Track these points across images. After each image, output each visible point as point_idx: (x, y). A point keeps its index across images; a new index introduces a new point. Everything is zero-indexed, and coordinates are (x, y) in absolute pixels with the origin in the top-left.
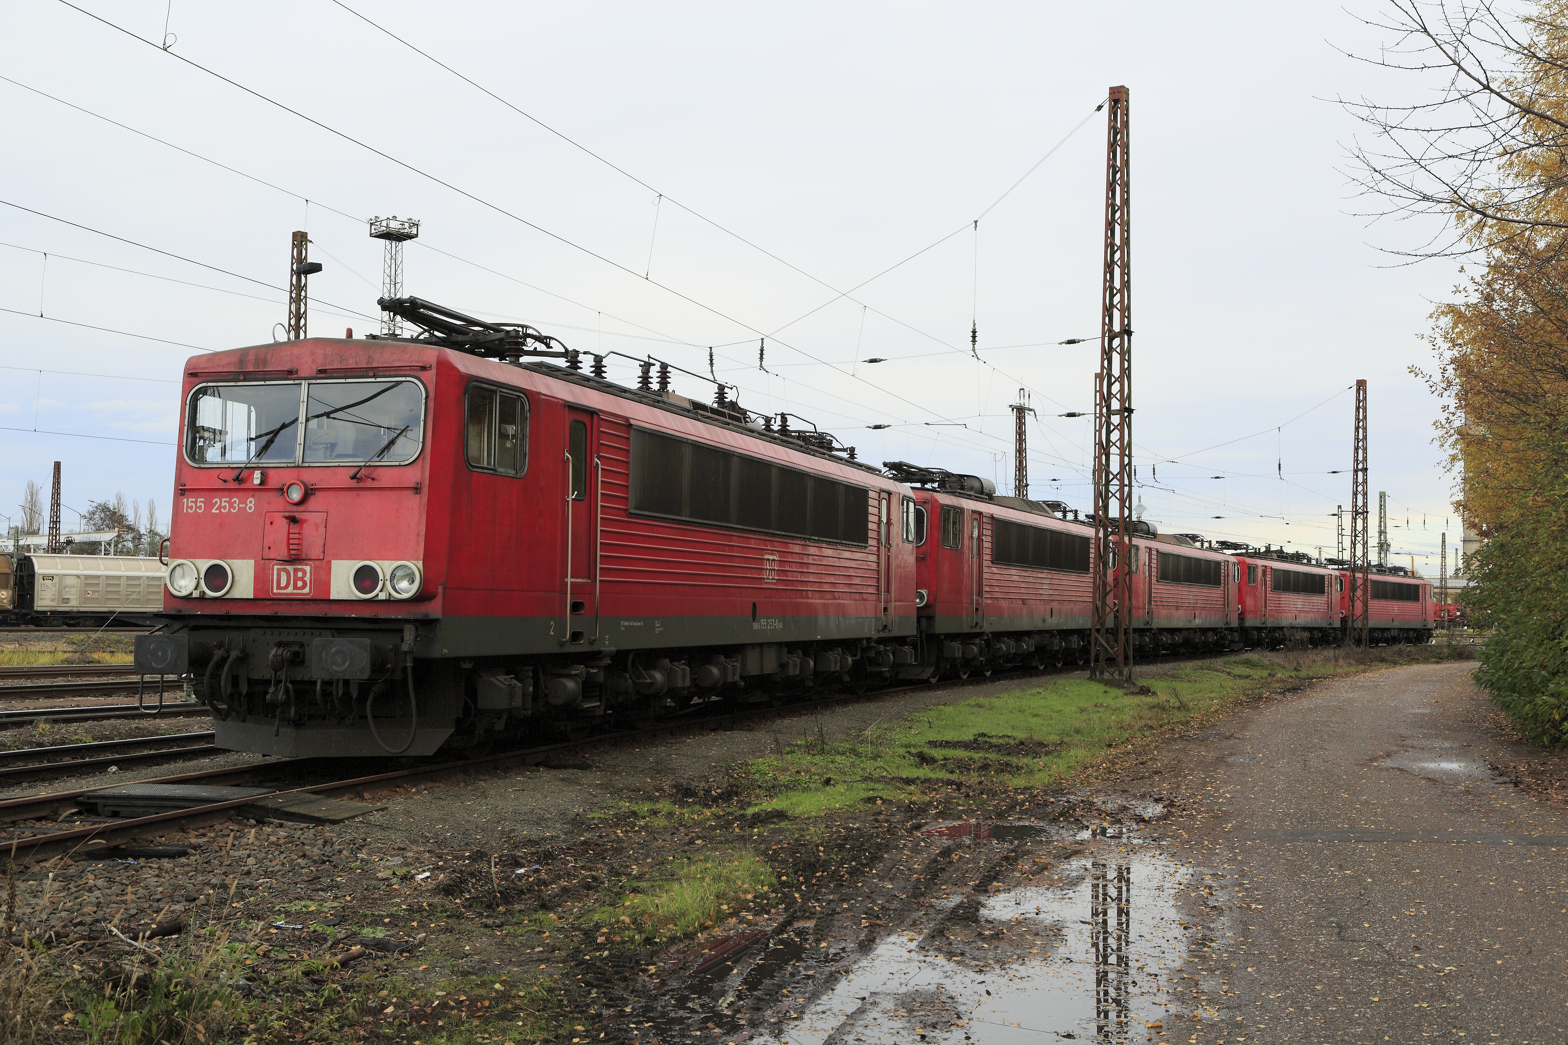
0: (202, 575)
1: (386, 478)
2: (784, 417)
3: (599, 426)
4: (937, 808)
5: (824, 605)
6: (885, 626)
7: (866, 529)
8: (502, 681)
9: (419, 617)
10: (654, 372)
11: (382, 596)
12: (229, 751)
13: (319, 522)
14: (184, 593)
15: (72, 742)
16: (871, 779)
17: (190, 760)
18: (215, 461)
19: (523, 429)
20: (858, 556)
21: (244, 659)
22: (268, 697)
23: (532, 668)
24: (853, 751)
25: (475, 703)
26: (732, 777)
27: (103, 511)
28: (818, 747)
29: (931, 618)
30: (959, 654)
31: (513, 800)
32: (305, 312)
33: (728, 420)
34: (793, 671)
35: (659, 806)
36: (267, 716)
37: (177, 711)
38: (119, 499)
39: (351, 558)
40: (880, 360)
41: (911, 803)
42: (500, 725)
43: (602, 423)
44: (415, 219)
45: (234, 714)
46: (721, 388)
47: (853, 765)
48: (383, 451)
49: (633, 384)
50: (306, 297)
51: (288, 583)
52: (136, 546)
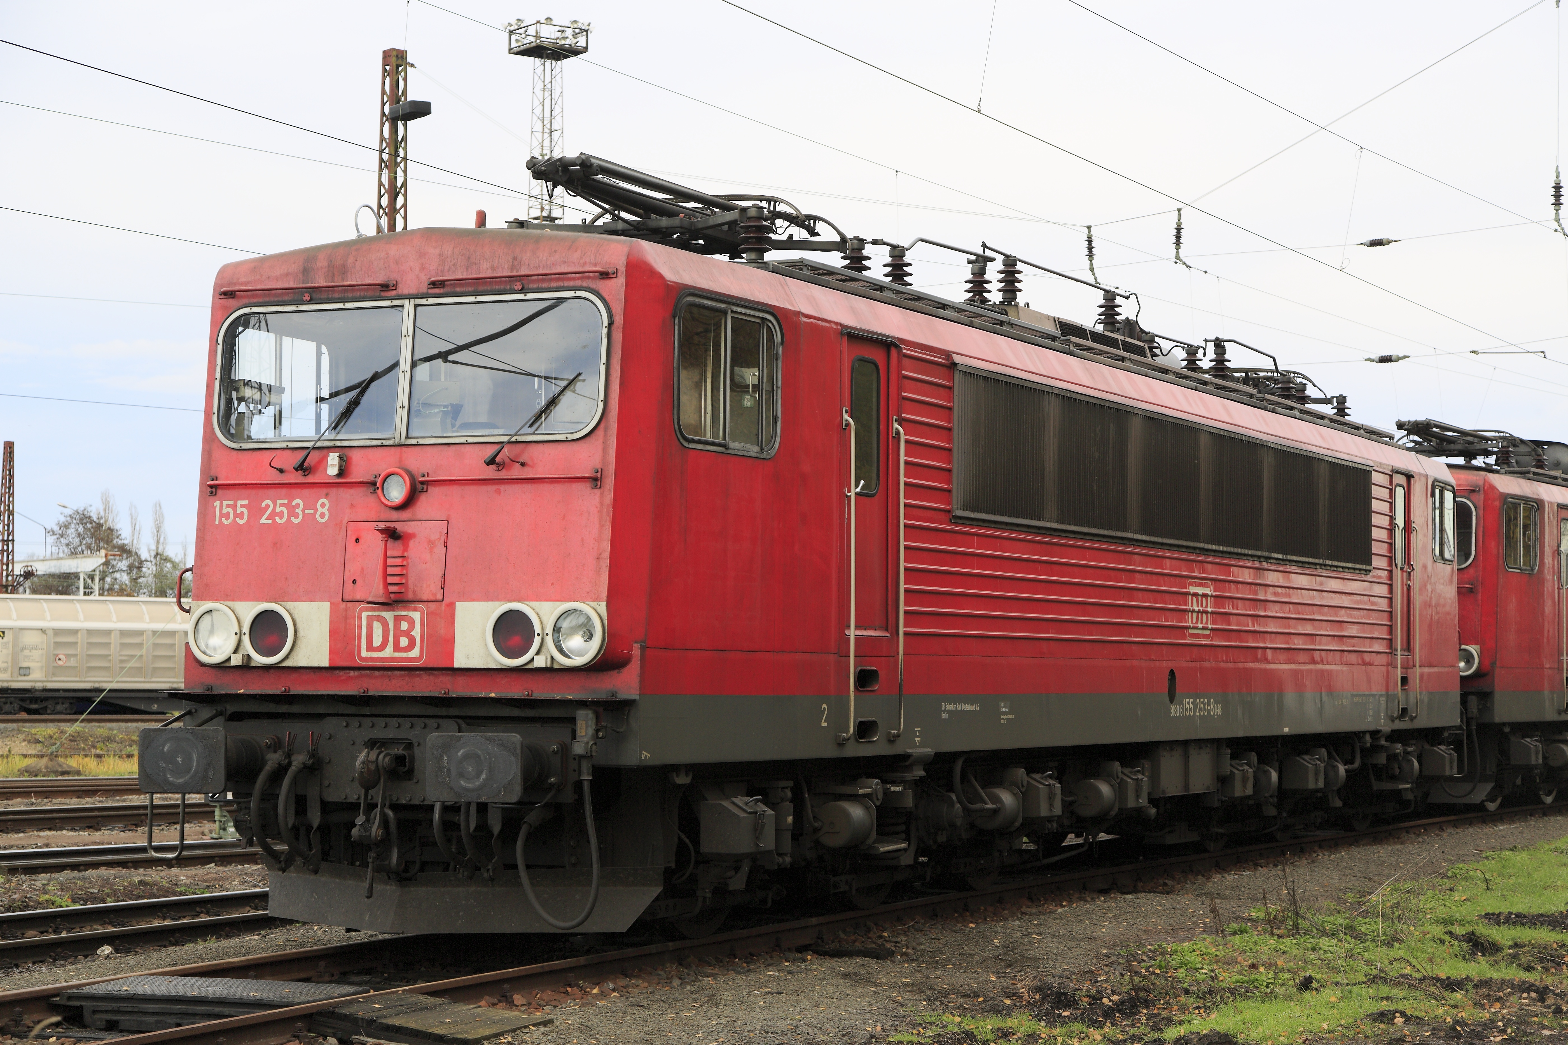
0: (246, 629)
1: (544, 462)
2: (1219, 345)
3: (900, 368)
4: (1504, 1031)
5: (1295, 672)
6: (1404, 711)
7: (1368, 539)
8: (741, 805)
9: (602, 696)
10: (993, 272)
11: (540, 662)
12: (290, 922)
13: (434, 537)
14: (217, 658)
15: (39, 905)
16: (1385, 980)
17: (228, 936)
18: (262, 437)
19: (771, 377)
20: (1354, 586)
21: (315, 768)
22: (355, 831)
23: (791, 783)
24: (1350, 930)
25: (697, 843)
26: (1137, 973)
27: (81, 521)
28: (1288, 922)
29: (1485, 696)
30: (1536, 760)
31: (763, 1009)
32: (404, 184)
33: (1122, 353)
34: (1242, 789)
35: (1011, 1023)
36: (352, 864)
37: (209, 856)
38: (106, 503)
39: (488, 597)
40: (1389, 242)
41: (1457, 1022)
42: (738, 882)
43: (906, 361)
44: (583, 22)
45: (299, 861)
46: (1110, 297)
47: (1350, 955)
48: (538, 417)
49: (957, 293)
50: (405, 159)
51: (389, 640)
52: (135, 580)
